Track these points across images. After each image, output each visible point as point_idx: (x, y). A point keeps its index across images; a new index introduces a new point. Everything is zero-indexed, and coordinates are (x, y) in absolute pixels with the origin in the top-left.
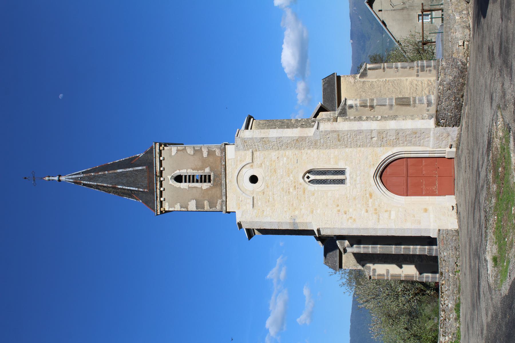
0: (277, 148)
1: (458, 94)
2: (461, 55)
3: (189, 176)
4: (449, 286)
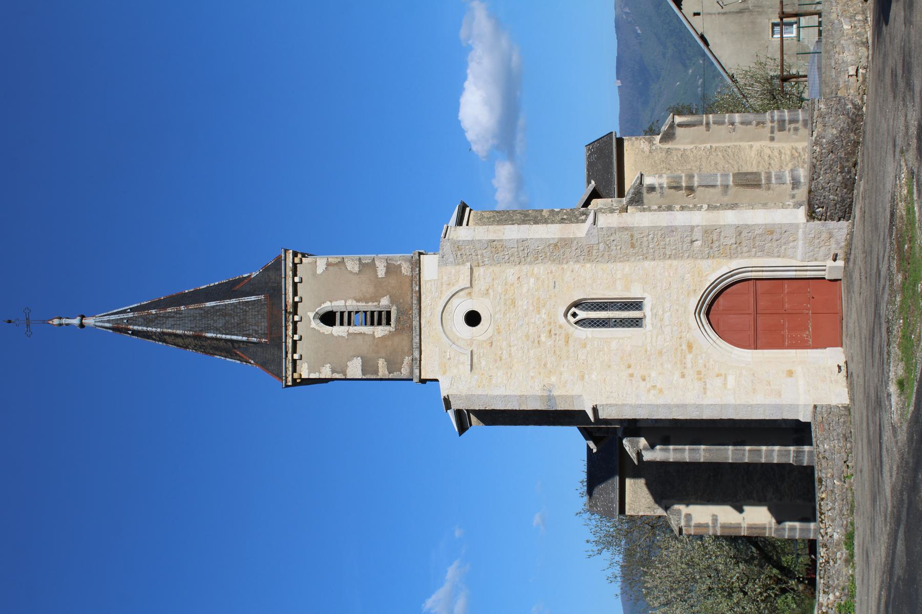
0: (517, 261)
1: (848, 161)
2: (852, 91)
3: (350, 313)
4: (834, 502)
